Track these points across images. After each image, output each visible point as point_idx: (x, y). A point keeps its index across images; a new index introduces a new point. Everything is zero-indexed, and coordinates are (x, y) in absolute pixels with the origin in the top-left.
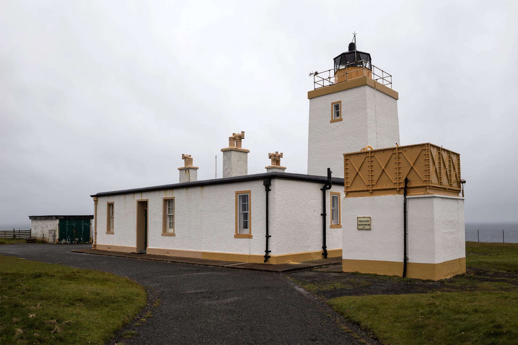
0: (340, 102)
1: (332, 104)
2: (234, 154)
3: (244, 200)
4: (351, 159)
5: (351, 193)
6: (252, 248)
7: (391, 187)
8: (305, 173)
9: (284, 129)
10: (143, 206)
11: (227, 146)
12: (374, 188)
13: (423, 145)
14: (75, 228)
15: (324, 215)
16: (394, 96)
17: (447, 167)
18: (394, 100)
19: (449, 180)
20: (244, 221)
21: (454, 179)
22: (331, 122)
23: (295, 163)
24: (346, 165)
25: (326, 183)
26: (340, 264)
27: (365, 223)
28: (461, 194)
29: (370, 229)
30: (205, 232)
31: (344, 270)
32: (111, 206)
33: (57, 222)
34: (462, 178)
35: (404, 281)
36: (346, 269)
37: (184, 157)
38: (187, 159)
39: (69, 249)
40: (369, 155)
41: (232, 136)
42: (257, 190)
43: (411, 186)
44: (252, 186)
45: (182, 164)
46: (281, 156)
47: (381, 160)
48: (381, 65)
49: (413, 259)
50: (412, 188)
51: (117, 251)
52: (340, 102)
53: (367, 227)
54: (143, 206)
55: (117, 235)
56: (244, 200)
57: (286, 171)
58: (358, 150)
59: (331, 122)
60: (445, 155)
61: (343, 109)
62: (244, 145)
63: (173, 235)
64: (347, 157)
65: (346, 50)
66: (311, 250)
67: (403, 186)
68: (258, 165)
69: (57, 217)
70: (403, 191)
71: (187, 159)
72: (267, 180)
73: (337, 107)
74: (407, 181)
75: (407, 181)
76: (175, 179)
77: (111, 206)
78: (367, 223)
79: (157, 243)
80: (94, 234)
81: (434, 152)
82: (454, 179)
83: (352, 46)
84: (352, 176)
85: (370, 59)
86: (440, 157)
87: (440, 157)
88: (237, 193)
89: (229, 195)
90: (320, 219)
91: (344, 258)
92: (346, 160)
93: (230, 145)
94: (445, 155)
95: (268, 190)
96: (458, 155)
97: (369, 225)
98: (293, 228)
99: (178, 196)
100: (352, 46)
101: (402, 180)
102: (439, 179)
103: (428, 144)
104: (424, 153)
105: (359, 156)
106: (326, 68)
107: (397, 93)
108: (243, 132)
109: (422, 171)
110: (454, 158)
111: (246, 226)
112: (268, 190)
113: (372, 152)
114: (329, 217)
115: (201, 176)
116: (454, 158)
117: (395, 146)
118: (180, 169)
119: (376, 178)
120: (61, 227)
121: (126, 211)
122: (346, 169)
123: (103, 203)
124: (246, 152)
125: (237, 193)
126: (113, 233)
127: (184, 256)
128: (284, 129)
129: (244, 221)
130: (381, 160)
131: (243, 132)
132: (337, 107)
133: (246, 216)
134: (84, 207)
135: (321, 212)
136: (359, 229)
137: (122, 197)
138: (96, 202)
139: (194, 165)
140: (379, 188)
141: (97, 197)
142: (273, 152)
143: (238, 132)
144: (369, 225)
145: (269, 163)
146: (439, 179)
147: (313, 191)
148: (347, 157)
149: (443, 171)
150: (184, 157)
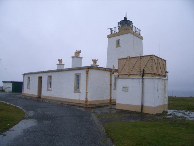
0: (120, 39)
1: (117, 40)
2: (76, 58)
3: (78, 77)
4: (121, 61)
5: (131, 75)
6: (80, 97)
7: (137, 73)
8: (106, 67)
9: (97, 50)
10: (40, 78)
11: (73, 55)
12: (130, 73)
13: (151, 55)
14: (18, 87)
15: (111, 85)
16: (141, 38)
17: (161, 65)
18: (141, 40)
19: (162, 71)
20: (77, 86)
21: (164, 71)
22: (116, 47)
23: (102, 63)
24: (119, 63)
25: (111, 71)
26: (115, 105)
27: (126, 88)
28: (166, 77)
29: (128, 91)
30: (64, 91)
31: (117, 108)
32: (29, 78)
33: (12, 84)
34: (167, 71)
35: (140, 115)
36: (117, 107)
37: (59, 60)
38: (60, 61)
39: (15, 94)
40: (129, 59)
41: (76, 51)
42: (83, 73)
43: (145, 73)
44: (80, 71)
45: (58, 62)
46: (97, 60)
47: (133, 62)
48: (136, 24)
49: (146, 104)
50: (145, 74)
51: (30, 96)
52: (120, 39)
53: (127, 90)
54: (40, 78)
55: (30, 90)
56: (78, 77)
57: (99, 66)
58: (125, 57)
59: (82, 58)
60: (160, 60)
61: (121, 42)
62: (81, 55)
63: (51, 90)
64: (119, 60)
65: (123, 19)
66: (105, 99)
67: (142, 73)
68: (86, 62)
69: (11, 82)
70: (142, 75)
71: (60, 61)
72: (88, 69)
73: (118, 41)
74: (144, 71)
75: (144, 71)
76: (55, 68)
77: (29, 78)
78: (127, 88)
79: (45, 93)
80: (163, 78)
81: (156, 59)
82: (164, 71)
83: (125, 18)
84: (121, 68)
85: (132, 23)
86: (158, 61)
87: (158, 61)
88: (75, 74)
89: (72, 74)
90: (109, 86)
91: (117, 102)
92: (119, 61)
93: (75, 55)
94: (160, 60)
95: (87, 73)
96: (165, 61)
97: (127, 89)
98: (93, 91)
99: (53, 75)
100: (125, 18)
101: (142, 70)
102: (157, 70)
103: (153, 55)
104: (151, 59)
105: (124, 59)
106: (115, 25)
107: (142, 37)
108: (80, 50)
109: (152, 68)
110: (164, 62)
111: (78, 87)
112: (87, 73)
113: (129, 58)
114: (113, 86)
115: (65, 67)
116: (164, 62)
117: (139, 56)
118: (57, 65)
119: (131, 69)
120: (13, 85)
121: (34, 81)
122: (119, 65)
123: (26, 77)
124: (81, 58)
125: (75, 74)
126: (29, 89)
127: (55, 99)
128: (97, 50)
129: (77, 86)
130: (133, 62)
131: (80, 50)
132: (118, 41)
133: (79, 84)
134: (20, 79)
135: (109, 83)
136: (123, 91)
137: (33, 75)
138: (24, 76)
139: (63, 63)
140: (132, 74)
141: (24, 75)
142: (94, 59)
143: (78, 50)
144: (127, 89)
145: (92, 63)
146: (157, 70)
147: (107, 74)
148: (119, 60)
149: (159, 67)
150: (59, 60)
